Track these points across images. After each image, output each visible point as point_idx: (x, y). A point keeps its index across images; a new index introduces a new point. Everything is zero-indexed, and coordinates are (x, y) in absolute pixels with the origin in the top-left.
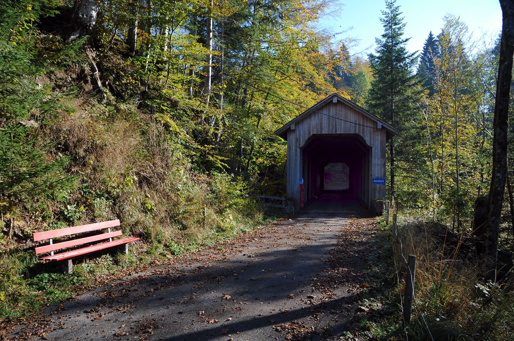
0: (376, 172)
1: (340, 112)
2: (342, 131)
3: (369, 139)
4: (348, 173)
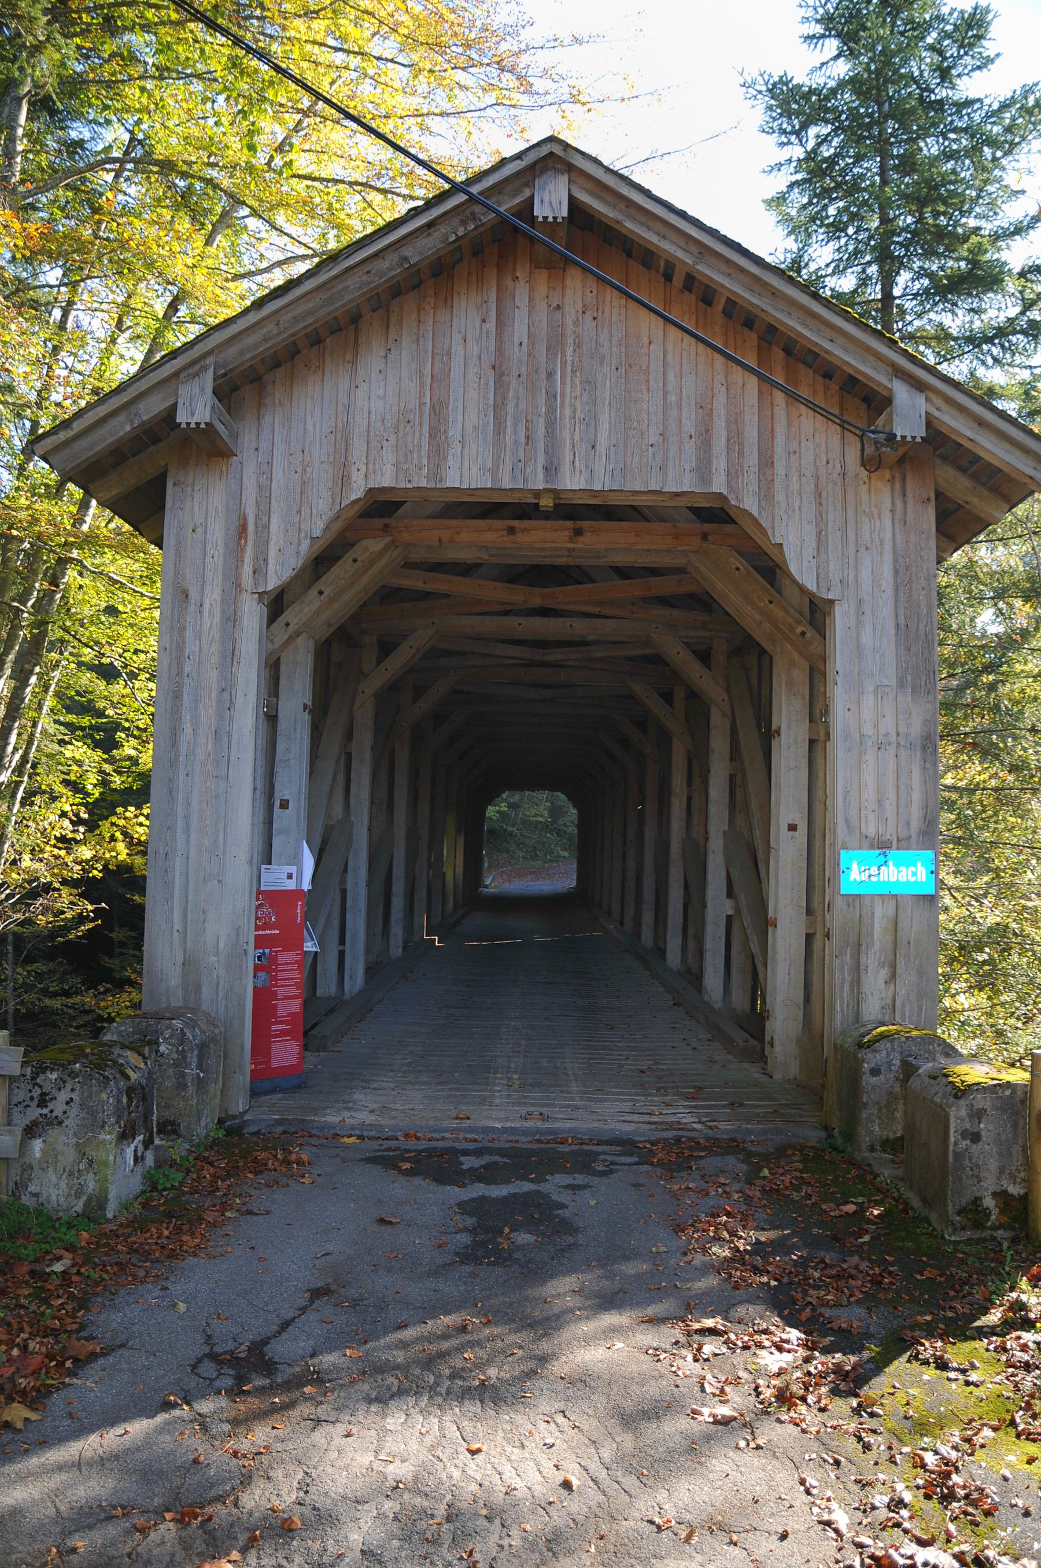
0: (869, 795)
1: (589, 323)
2: (599, 469)
3: (811, 541)
4: (573, 830)
